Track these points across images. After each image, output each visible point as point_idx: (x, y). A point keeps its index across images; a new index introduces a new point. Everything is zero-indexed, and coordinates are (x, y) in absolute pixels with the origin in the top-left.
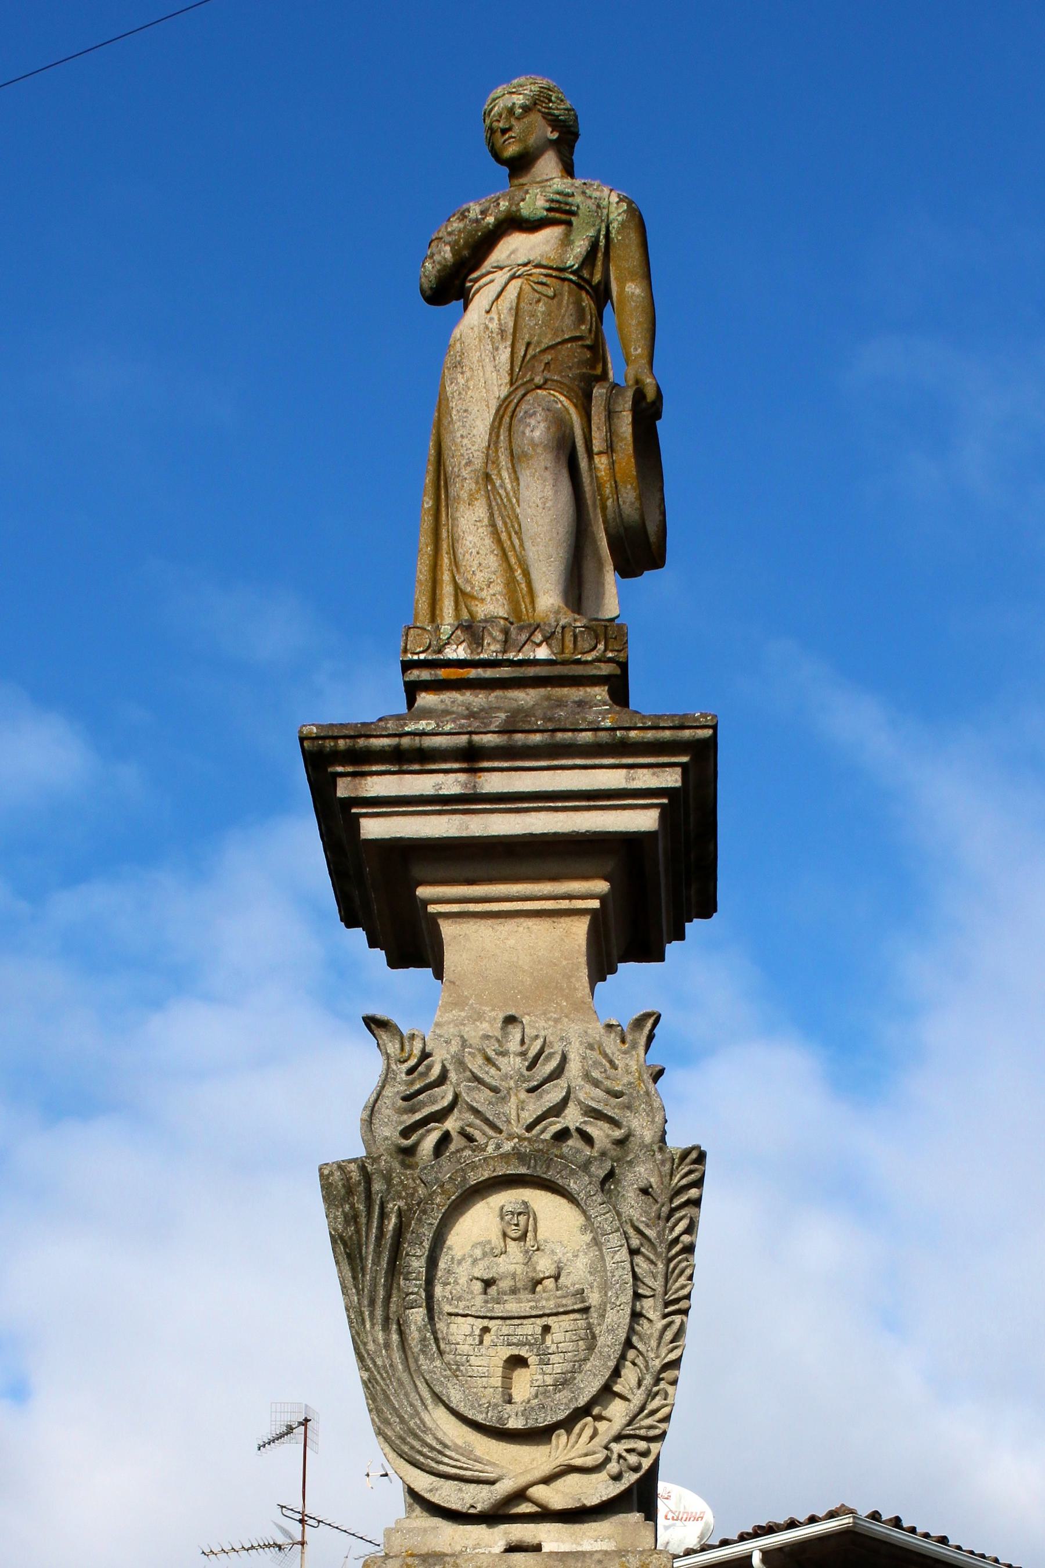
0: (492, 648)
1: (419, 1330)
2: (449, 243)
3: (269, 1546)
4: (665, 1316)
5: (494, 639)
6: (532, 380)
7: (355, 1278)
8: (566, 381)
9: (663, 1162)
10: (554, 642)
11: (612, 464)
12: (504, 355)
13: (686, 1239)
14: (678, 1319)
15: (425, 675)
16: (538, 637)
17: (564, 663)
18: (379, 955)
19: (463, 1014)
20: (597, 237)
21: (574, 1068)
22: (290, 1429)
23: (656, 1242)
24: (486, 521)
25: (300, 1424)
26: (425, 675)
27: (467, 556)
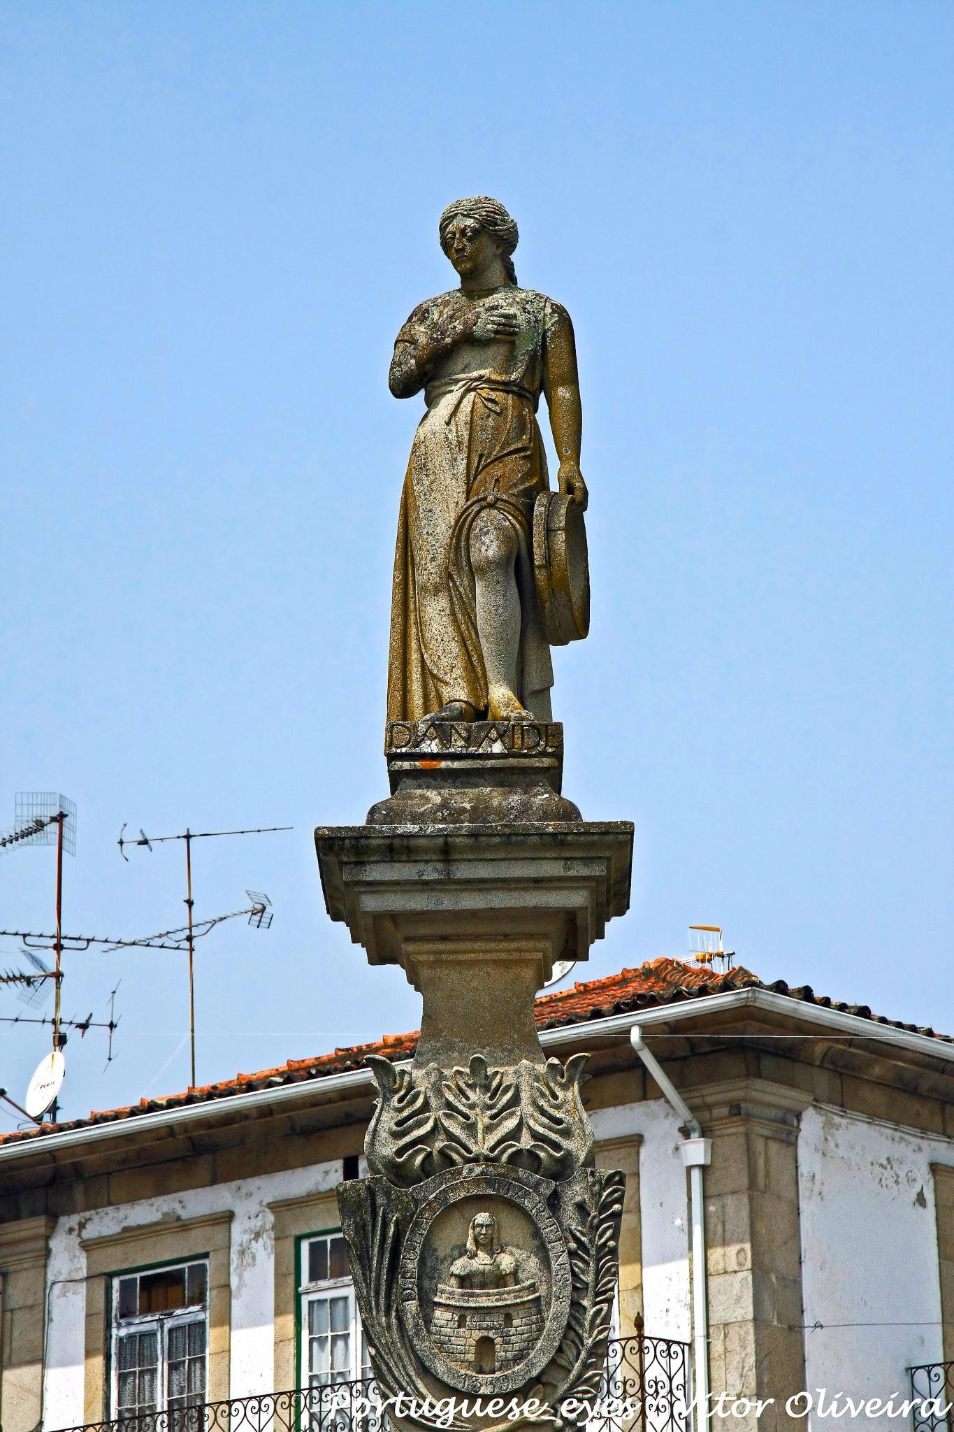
0: (458, 743)
1: (414, 1317)
2: (414, 357)
3: (14, 979)
4: (595, 1304)
5: (460, 735)
6: (485, 499)
7: (364, 1274)
8: (513, 500)
9: (594, 1184)
10: (506, 740)
11: (550, 575)
12: (462, 467)
13: (612, 1243)
14: (605, 1306)
15: (406, 765)
16: (494, 734)
17: (514, 756)
18: (360, 952)
19: (439, 1044)
20: (535, 351)
21: (525, 1096)
22: (40, 825)
23: (589, 1246)
24: (448, 612)
25: (53, 819)
26: (406, 765)
27: (434, 642)
